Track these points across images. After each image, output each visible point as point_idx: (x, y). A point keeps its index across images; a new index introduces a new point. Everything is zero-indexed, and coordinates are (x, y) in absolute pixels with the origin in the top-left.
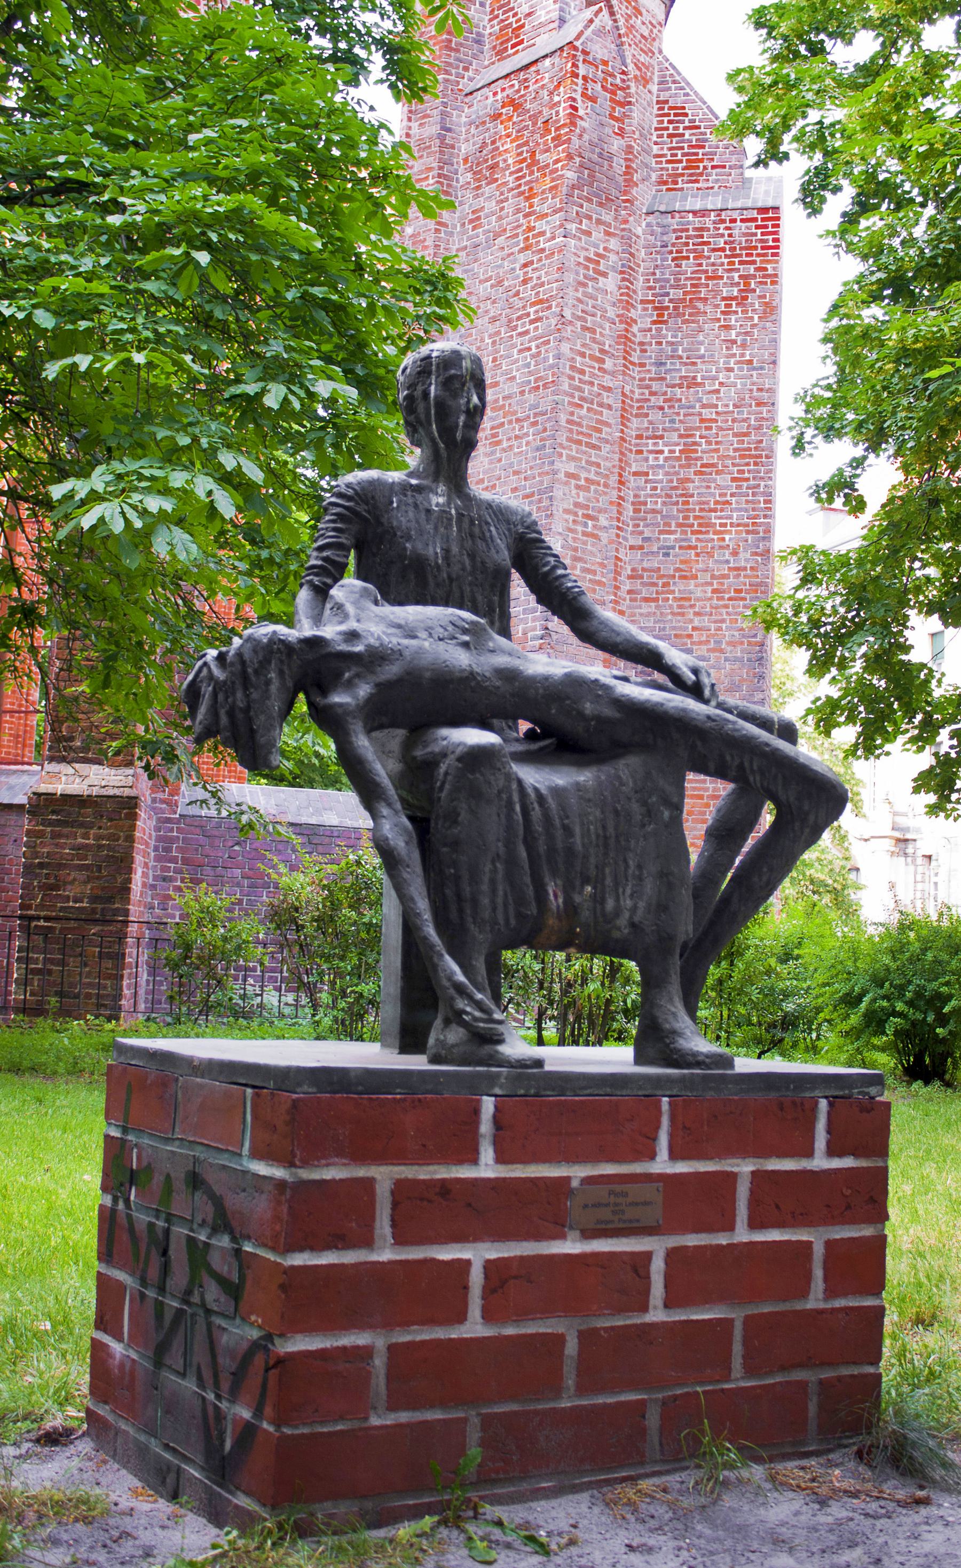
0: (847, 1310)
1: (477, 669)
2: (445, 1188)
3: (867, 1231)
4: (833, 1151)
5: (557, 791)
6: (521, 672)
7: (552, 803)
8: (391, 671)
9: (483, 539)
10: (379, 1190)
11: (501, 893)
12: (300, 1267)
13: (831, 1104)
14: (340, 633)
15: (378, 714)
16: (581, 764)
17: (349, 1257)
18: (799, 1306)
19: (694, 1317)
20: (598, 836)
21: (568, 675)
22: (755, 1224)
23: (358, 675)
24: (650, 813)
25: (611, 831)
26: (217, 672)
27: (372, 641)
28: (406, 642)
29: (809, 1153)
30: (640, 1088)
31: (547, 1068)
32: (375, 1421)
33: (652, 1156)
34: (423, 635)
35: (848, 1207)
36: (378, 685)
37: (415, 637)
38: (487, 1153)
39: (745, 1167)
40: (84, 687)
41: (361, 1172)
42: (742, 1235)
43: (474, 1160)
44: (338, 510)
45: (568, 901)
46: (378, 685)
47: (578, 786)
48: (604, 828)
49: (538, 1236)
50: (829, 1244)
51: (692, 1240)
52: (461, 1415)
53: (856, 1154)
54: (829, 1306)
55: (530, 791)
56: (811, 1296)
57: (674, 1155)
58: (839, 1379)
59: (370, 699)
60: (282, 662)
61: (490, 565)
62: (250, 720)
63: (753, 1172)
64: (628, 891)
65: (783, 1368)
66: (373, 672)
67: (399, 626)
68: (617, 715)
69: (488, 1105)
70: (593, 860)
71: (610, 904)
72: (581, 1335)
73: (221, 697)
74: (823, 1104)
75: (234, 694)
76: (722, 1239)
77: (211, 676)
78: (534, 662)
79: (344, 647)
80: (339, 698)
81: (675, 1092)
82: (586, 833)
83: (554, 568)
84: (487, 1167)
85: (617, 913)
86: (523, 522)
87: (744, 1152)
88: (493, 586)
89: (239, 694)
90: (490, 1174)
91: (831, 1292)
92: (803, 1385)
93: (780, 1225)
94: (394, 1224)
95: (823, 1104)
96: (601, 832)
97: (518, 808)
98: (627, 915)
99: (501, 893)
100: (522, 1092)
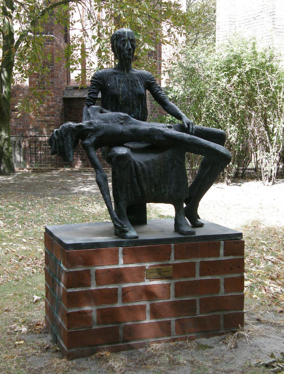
0: (232, 296)
1: (124, 130)
4: (225, 254)
5: (147, 163)
6: (138, 129)
7: (145, 166)
8: (100, 133)
11: (129, 192)
12: (71, 292)
13: (225, 242)
14: (87, 123)
15: (97, 145)
16: (156, 153)
17: (84, 289)
18: (216, 295)
19: (184, 299)
21: (150, 129)
22: (201, 275)
23: (92, 135)
26: (56, 137)
28: (105, 124)
30: (165, 242)
31: (139, 239)
33: (169, 259)
34: (110, 121)
35: (231, 269)
36: (97, 137)
37: (108, 123)
39: (198, 260)
40: (147, 47)
42: (198, 278)
44: (94, 83)
46: (97, 137)
47: (153, 160)
48: (161, 171)
50: (226, 280)
52: (117, 325)
53: (233, 255)
54: (226, 295)
55: (138, 164)
56: (220, 292)
57: (176, 258)
59: (95, 141)
60: (71, 133)
62: (64, 149)
63: (200, 262)
64: (168, 187)
65: (212, 312)
66: (96, 134)
67: (104, 120)
68: (165, 139)
73: (57, 143)
74: (222, 242)
75: (60, 142)
76: (192, 279)
77: (54, 138)
78: (143, 125)
79: (88, 127)
80: (87, 142)
81: (176, 242)
83: (158, 91)
86: (148, 78)
87: (197, 256)
89: (61, 143)
90: (122, 266)
91: (226, 292)
93: (210, 274)
95: (222, 242)
97: (134, 169)
98: (168, 193)
99: (129, 192)
100: (130, 245)
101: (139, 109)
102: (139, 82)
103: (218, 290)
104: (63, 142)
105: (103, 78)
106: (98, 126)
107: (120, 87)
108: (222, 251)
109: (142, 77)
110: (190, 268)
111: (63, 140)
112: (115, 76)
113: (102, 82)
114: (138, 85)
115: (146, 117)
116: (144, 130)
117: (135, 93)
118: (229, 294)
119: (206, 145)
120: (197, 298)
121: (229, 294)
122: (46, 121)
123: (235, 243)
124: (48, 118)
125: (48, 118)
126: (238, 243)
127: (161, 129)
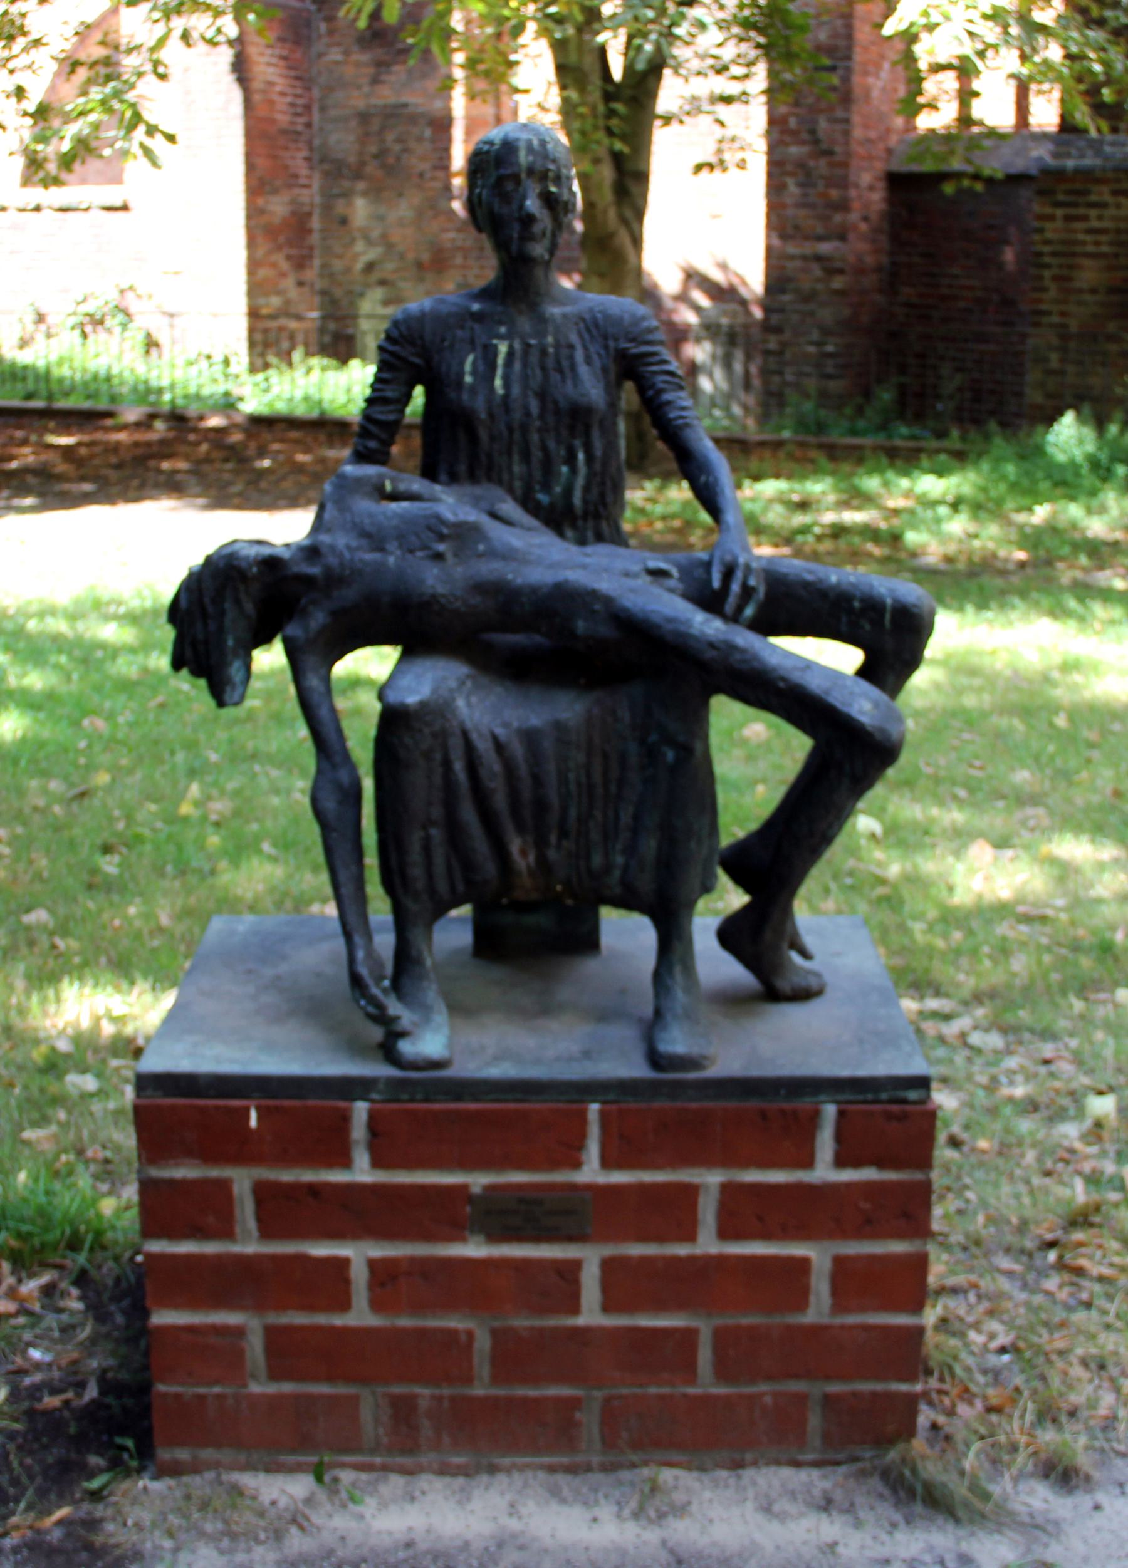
2: (315, 1190)
3: (898, 1247)
4: (841, 1161)
8: (349, 595)
9: (560, 370)
10: (236, 1189)
17: (211, 1248)
20: (579, 784)
24: (651, 754)
25: (597, 777)
27: (332, 561)
29: (808, 1162)
32: (255, 1388)
34: (392, 546)
36: (334, 614)
37: (381, 549)
38: (362, 1158)
39: (712, 1179)
41: (214, 1173)
43: (346, 1162)
45: (542, 859)
47: (559, 726)
48: (589, 776)
49: (429, 1237)
50: (840, 1264)
51: (636, 1250)
53: (881, 1163)
54: (838, 1320)
55: (483, 746)
57: (607, 1163)
58: (855, 1394)
61: (563, 404)
69: (361, 1109)
70: (573, 813)
71: (597, 860)
72: (495, 1333)
76: (682, 1250)
81: (611, 1097)
82: (563, 780)
84: (362, 1171)
85: (608, 869)
88: (572, 429)
92: (801, 1399)
93: (766, 1235)
94: (259, 1219)
96: (583, 780)
98: (617, 873)
101: (574, 470)
102: (579, 356)
103: (800, 1301)
104: (206, 625)
105: (421, 337)
106: (341, 564)
107: (493, 373)
108: (825, 1143)
109: (597, 325)
110: (672, 1211)
111: (204, 615)
112: (472, 329)
113: (418, 355)
114: (573, 367)
115: (609, 498)
116: (534, 590)
117: (556, 402)
118: (852, 1319)
119: (783, 679)
120: (704, 1326)
121: (852, 1319)
122: (818, 258)
123: (889, 1116)
124: (825, 248)
125: (825, 248)
126: (903, 1117)
127: (605, 585)
